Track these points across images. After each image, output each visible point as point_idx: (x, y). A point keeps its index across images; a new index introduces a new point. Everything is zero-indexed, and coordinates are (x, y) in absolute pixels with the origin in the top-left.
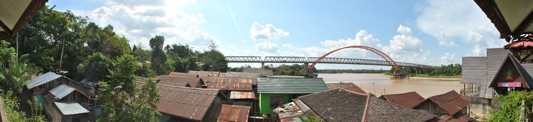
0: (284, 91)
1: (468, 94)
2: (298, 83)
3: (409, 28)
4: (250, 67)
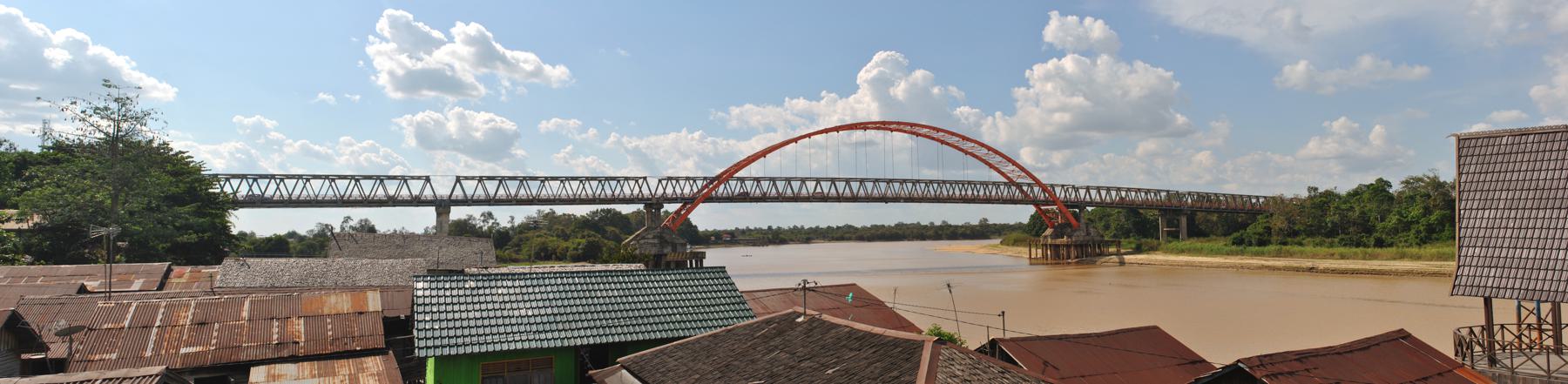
0: (549, 335)
1: (1517, 361)
2: (616, 293)
3: (1100, 23)
4: (372, 230)
